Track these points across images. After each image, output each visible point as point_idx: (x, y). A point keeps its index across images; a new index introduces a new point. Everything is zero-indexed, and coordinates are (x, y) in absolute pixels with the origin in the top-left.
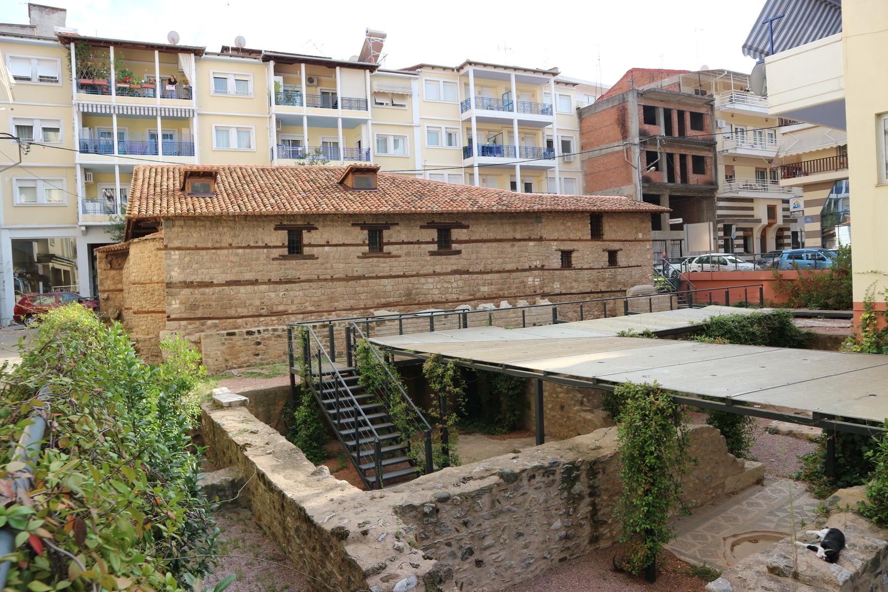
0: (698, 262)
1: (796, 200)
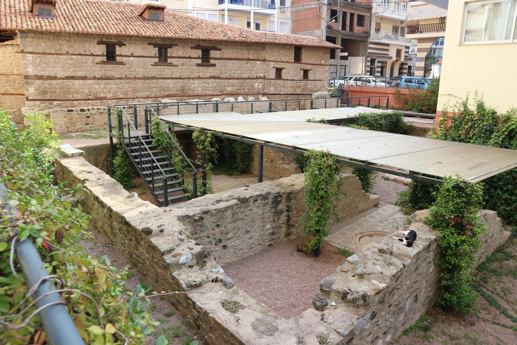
0: (354, 80)
1: (413, 47)
